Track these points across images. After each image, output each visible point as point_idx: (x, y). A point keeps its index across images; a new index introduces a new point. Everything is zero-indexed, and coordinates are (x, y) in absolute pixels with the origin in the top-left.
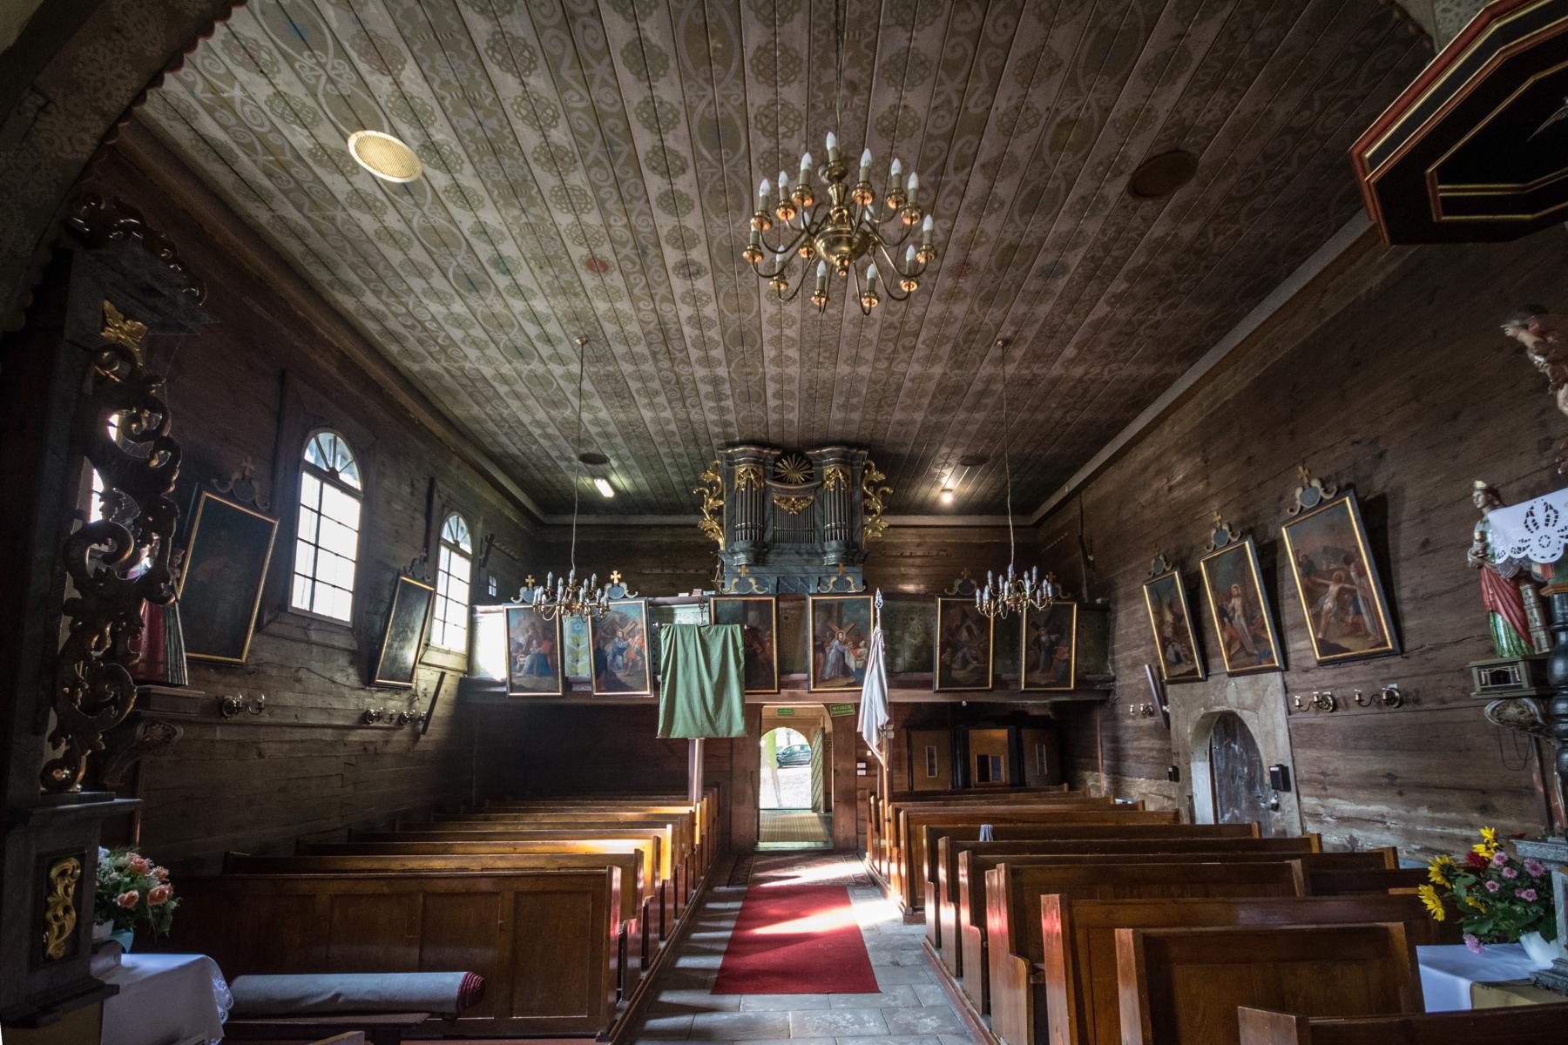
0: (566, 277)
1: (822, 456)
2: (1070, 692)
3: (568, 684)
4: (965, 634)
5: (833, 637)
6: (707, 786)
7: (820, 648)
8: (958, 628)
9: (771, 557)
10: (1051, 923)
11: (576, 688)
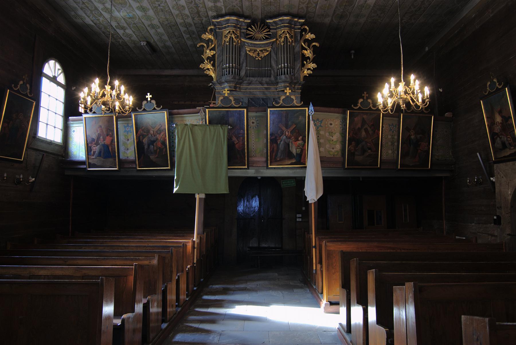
2: (378, 168)
3: (122, 163)
4: (363, 133)
6: (206, 225)
8: (359, 129)
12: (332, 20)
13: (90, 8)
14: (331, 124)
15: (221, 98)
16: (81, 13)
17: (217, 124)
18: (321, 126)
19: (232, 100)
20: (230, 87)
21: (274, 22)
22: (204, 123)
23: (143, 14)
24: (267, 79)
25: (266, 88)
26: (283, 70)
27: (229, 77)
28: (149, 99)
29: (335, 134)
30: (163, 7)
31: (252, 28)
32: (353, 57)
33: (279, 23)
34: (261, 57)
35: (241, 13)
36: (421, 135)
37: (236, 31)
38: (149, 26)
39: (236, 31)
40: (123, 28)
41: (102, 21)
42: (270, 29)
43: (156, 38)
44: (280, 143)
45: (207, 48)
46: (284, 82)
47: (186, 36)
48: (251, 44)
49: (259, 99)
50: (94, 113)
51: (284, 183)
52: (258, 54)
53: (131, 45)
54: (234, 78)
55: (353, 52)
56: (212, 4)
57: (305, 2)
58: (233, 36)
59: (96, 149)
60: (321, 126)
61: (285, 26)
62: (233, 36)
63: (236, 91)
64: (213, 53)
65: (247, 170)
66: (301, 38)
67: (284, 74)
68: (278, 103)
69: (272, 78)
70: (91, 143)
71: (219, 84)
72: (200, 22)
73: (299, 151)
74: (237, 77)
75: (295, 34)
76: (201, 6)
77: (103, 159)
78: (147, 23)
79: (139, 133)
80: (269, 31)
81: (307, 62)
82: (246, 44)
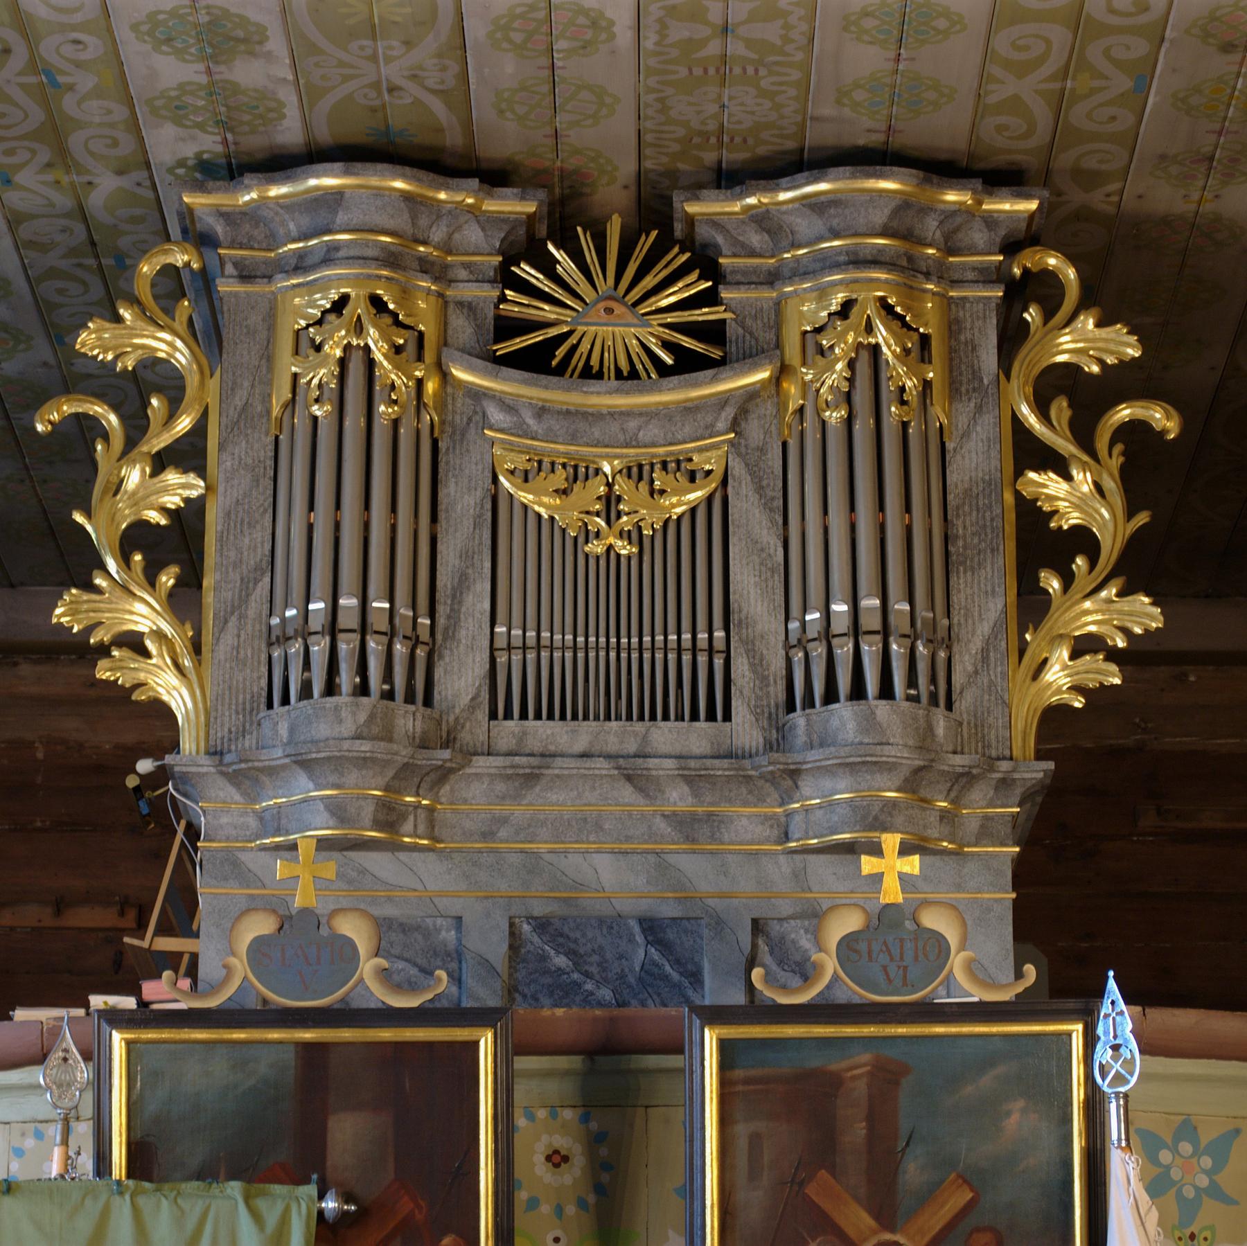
15: (259, 926)
17: (207, 1174)
18: (1215, 1192)
19: (363, 946)
20: (337, 811)
21: (762, 219)
22: (86, 1163)
24: (697, 737)
25: (687, 826)
26: (844, 651)
31: (548, 267)
33: (805, 225)
34: (635, 536)
35: (453, 139)
37: (405, 294)
39: (405, 294)
42: (711, 270)
45: (131, 443)
46: (859, 765)
48: (542, 412)
49: (611, 924)
52: (610, 503)
56: (191, 72)
57: (1041, 60)
58: (375, 340)
60: (1215, 1192)
61: (857, 260)
62: (375, 340)
63: (394, 847)
64: (179, 487)
67: (858, 692)
68: (805, 972)
69: (744, 729)
71: (235, 778)
72: (64, 201)
75: (953, 327)
76: (86, 82)
81: (1068, 579)
82: (496, 415)
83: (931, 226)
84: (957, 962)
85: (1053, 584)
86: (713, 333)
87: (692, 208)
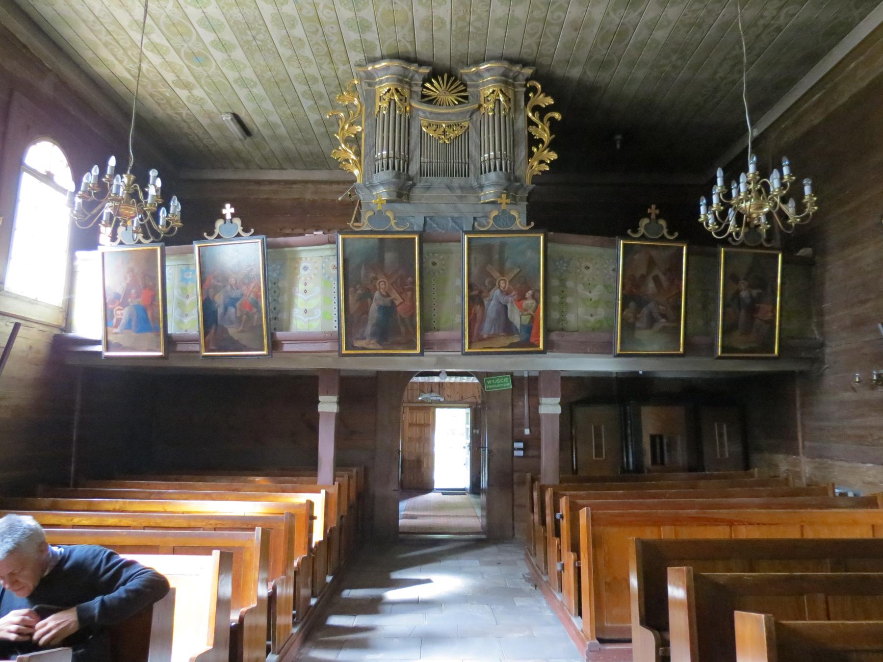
0: (260, 37)
1: (478, 74)
2: (775, 358)
3: (170, 342)
4: (651, 286)
5: (493, 285)
6: (340, 464)
7: (476, 299)
8: (644, 277)
9: (417, 192)
10: (676, 592)
11: (180, 347)
12: (585, 73)
13: (121, 42)
14: (587, 268)
15: (370, 214)
16: (104, 53)
23: (225, 56)
27: (385, 175)
28: (229, 217)
29: (595, 286)
30: (262, 41)
31: (432, 84)
32: (618, 146)
34: (450, 139)
35: (412, 55)
36: (760, 291)
38: (236, 81)
39: (403, 88)
40: (187, 86)
41: (147, 70)
42: (465, 85)
43: (250, 106)
44: (489, 305)
47: (307, 103)
48: (431, 113)
50: (121, 243)
51: (489, 382)
52: (444, 132)
53: (205, 122)
54: (398, 176)
55: (619, 137)
59: (122, 314)
65: (421, 358)
66: (526, 105)
67: (495, 169)
70: (113, 302)
71: (368, 188)
73: (526, 319)
74: (404, 177)
77: (134, 334)
78: (232, 75)
79: (207, 282)
80: (465, 91)
81: (538, 149)
82: (421, 114)
83: (511, 74)
84: (518, 221)
85: (535, 150)
86: (466, 98)
87: (462, 71)
